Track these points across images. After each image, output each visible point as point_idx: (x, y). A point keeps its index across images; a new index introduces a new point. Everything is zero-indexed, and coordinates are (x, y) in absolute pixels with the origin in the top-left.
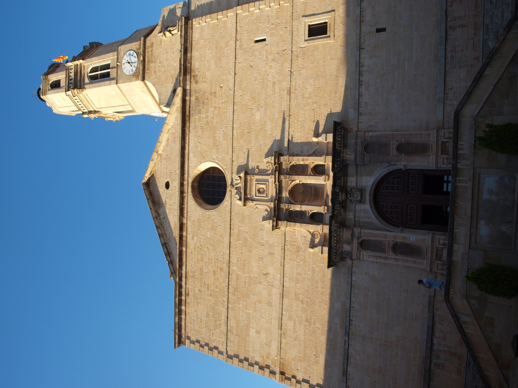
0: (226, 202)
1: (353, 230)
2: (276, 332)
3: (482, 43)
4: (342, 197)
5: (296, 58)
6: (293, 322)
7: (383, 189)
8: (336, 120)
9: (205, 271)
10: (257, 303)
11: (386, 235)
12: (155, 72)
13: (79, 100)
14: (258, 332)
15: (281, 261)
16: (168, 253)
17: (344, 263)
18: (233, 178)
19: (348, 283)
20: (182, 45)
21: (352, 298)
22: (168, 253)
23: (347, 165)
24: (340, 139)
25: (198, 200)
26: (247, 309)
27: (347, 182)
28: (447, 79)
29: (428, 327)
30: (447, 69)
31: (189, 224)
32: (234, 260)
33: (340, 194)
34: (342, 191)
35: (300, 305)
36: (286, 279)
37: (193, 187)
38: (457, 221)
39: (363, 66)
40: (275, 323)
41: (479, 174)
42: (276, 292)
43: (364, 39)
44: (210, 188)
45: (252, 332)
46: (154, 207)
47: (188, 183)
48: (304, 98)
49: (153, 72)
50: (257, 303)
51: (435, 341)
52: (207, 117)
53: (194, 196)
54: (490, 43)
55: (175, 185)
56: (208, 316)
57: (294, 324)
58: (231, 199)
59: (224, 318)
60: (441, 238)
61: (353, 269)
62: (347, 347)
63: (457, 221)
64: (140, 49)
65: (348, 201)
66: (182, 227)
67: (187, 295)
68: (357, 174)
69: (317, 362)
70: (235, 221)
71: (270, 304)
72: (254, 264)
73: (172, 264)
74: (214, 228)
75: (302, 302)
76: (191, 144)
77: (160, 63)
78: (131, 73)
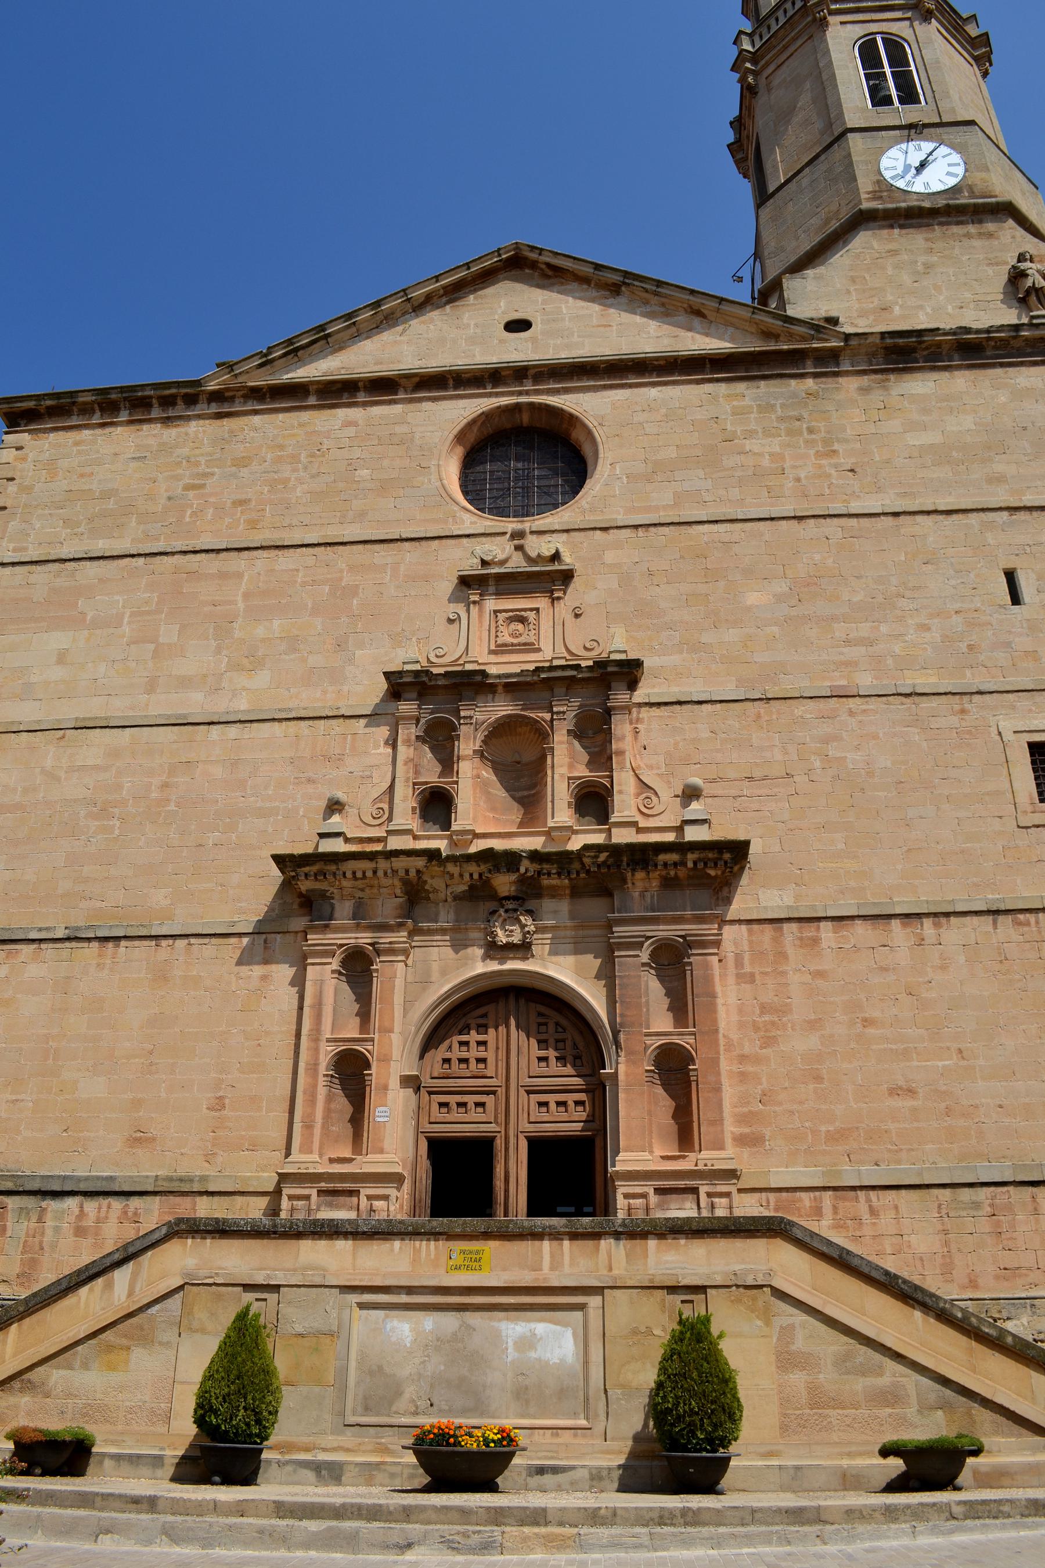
0: (471, 520)
1: (401, 925)
2: (69, 712)
3: (1023, 1295)
4: (504, 883)
5: (957, 707)
6: (99, 762)
7: (540, 1014)
8: (753, 849)
9: (244, 472)
10: (152, 646)
11: (391, 1031)
12: (893, 253)
13: (790, 13)
14: (62, 658)
15: (290, 710)
16: (296, 350)
17: (295, 906)
18: (550, 533)
19: (233, 924)
20: (988, 331)
21: (184, 942)
22: (296, 350)
23: (610, 894)
24: (690, 865)
25: (475, 429)
26: (132, 614)
27: (553, 897)
28: (903, 1192)
29: (111, 1178)
30: (935, 1192)
31: (398, 408)
32: (286, 560)
33: (513, 877)
34: (523, 880)
35: (156, 781)
36: (233, 731)
37: (517, 407)
38: (428, 1246)
39: (937, 925)
40: (93, 708)
41: (582, 1307)
42: (196, 703)
43: (1028, 924)
44: (528, 450)
45: (59, 640)
46: (444, 287)
47: (527, 393)
48: (826, 740)
49: (890, 247)
50: (152, 646)
51: (72, 1203)
52: (750, 434)
53: (487, 417)
54: (1025, 1320)
55: (518, 350)
56: (106, 495)
57: (96, 768)
58: (491, 540)
59: (101, 546)
60: (395, 1205)
61: (278, 936)
62: (33, 935)
63: (428, 1246)
64: (973, 194)
65: (492, 905)
66: (383, 387)
67: (167, 421)
68: (581, 927)
69: (162, 1310)
70: (410, 554)
71: (151, 687)
72: (276, 623)
73: (261, 366)
74: (384, 487)
75: (165, 785)
76: (654, 392)
77: (928, 266)
78: (888, 175)
